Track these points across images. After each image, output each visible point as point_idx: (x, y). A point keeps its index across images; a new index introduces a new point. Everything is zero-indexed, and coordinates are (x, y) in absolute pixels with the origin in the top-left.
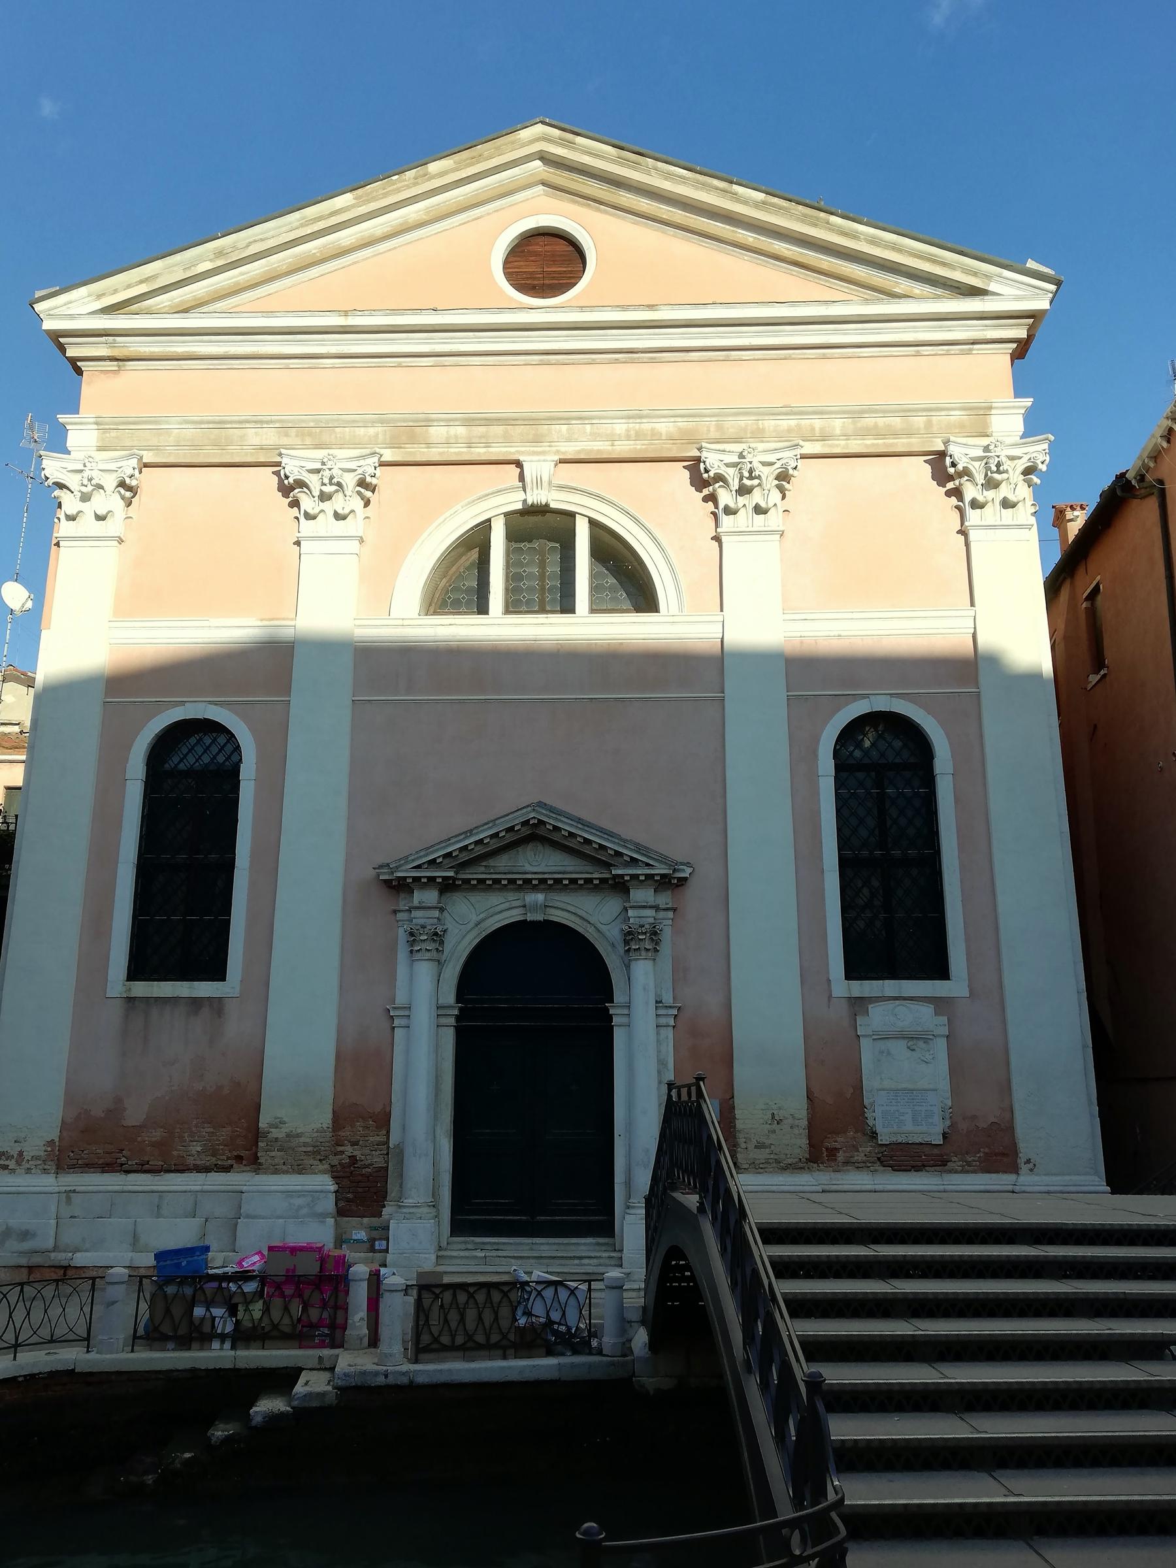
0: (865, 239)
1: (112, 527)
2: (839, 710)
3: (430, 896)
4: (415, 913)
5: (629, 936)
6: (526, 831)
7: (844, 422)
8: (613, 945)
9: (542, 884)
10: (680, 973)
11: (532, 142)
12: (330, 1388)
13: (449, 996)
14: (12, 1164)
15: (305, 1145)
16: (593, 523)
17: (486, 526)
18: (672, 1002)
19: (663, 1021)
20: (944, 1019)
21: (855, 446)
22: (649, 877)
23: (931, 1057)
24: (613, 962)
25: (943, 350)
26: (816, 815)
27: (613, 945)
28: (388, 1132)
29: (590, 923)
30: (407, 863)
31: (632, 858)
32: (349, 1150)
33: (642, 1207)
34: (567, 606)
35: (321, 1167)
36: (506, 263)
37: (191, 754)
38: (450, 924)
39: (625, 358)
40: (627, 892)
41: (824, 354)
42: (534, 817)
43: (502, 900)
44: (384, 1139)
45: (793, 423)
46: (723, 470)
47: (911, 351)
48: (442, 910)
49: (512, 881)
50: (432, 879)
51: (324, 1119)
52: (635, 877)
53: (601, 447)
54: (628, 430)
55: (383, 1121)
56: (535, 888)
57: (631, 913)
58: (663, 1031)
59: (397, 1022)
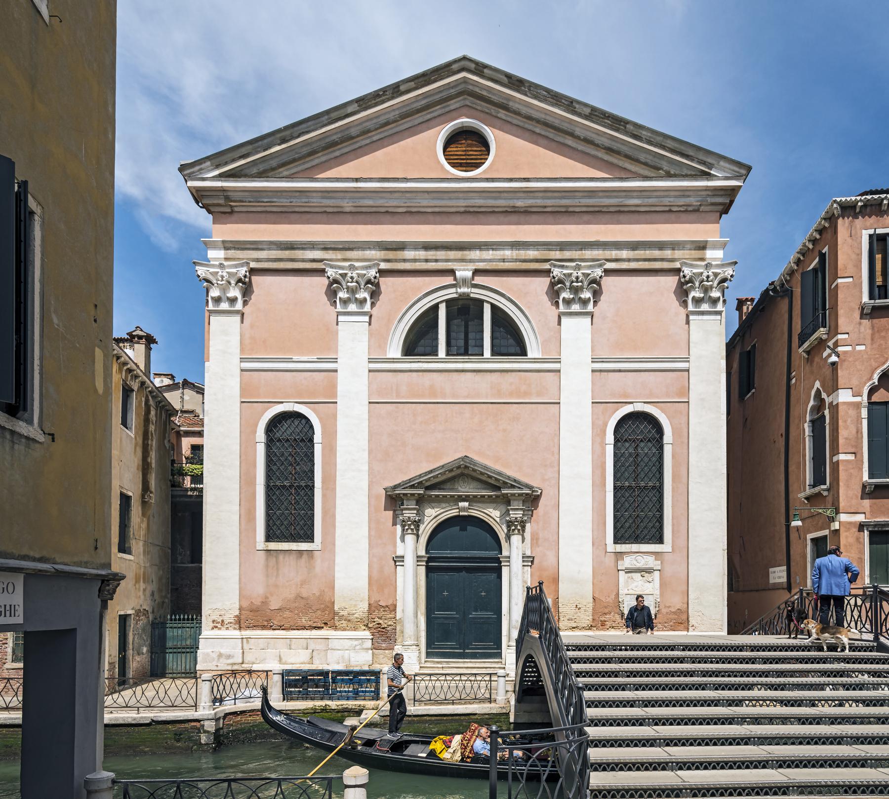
6: (459, 471)
14: (219, 625)
17: (435, 308)
26: (604, 464)
50: (413, 495)
51: (365, 606)
52: (513, 495)
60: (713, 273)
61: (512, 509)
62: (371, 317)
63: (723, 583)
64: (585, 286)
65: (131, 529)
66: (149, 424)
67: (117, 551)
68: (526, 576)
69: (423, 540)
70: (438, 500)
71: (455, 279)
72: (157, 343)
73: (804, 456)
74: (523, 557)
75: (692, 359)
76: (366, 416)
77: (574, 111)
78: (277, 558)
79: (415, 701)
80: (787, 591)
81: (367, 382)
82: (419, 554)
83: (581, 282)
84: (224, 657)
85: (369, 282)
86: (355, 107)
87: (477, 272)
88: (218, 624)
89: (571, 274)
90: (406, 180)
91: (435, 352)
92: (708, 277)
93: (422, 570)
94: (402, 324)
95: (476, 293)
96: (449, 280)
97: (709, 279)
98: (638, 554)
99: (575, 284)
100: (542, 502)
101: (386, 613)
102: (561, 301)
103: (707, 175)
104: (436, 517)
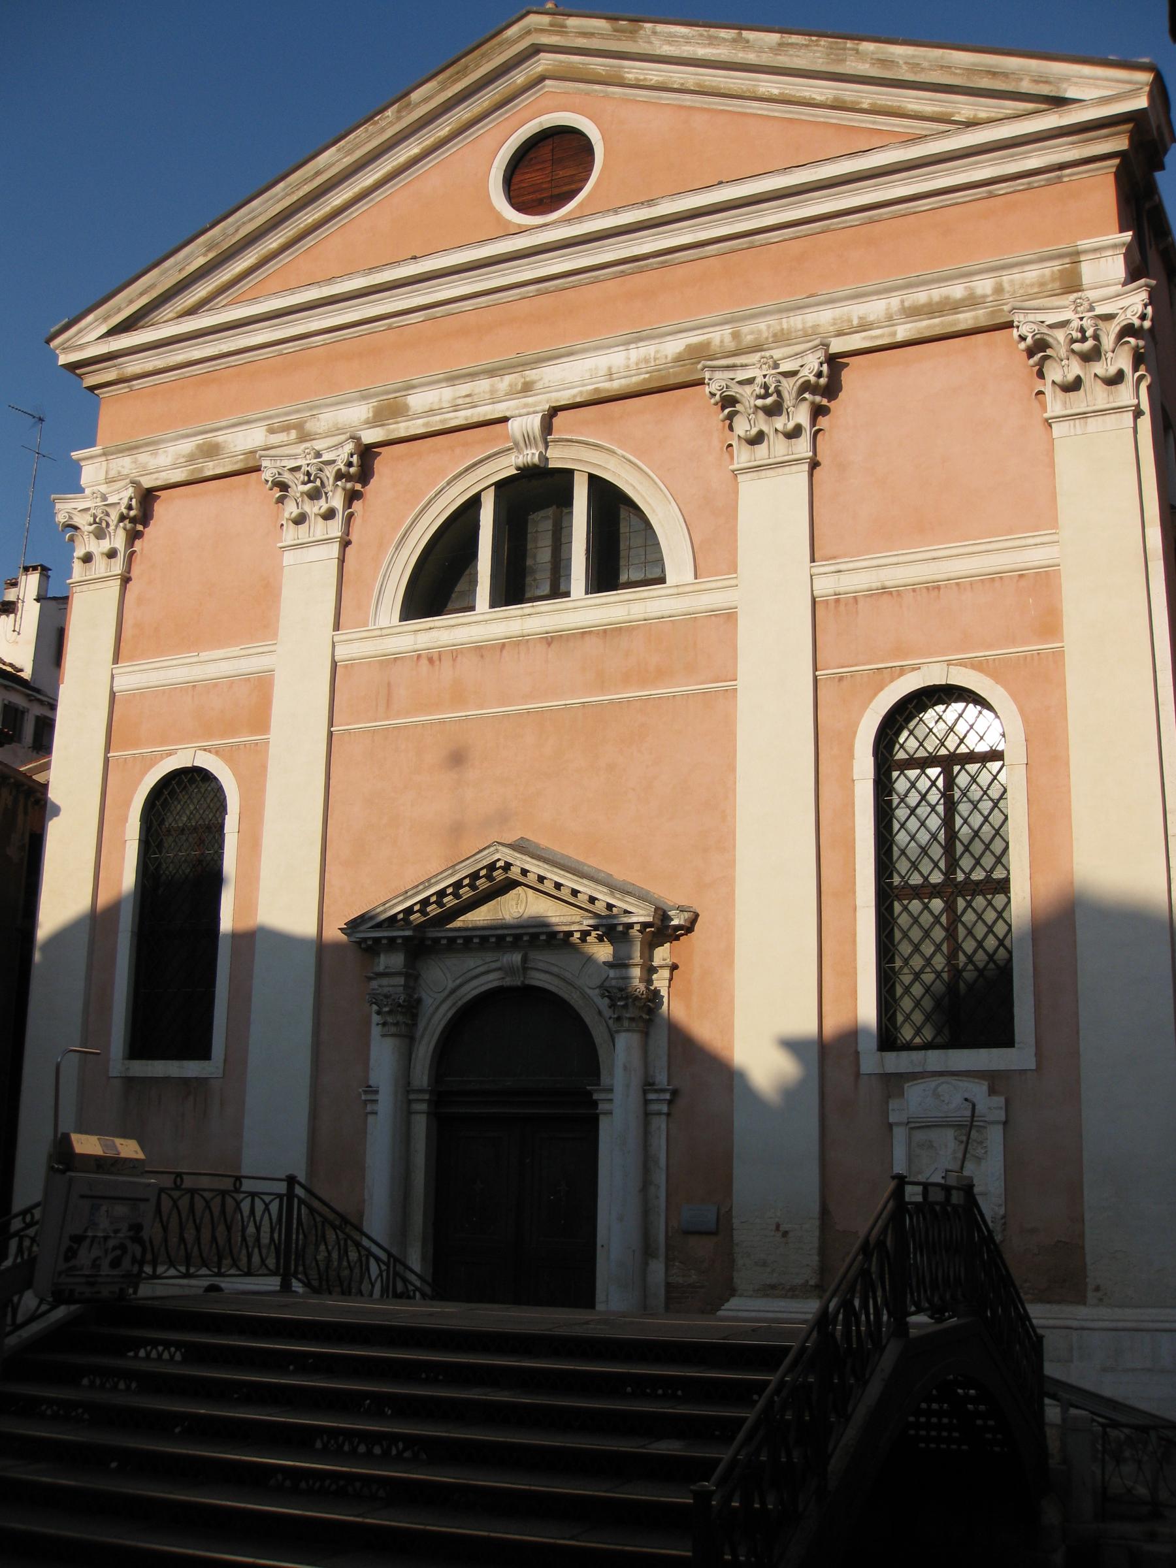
2: (882, 689)
7: (889, 303)
11: (521, 37)
16: (593, 479)
17: (474, 503)
18: (666, 1084)
20: (999, 1100)
23: (983, 1152)
24: (599, 1034)
25: (1023, 184)
29: (575, 988)
33: (423, 1100)
34: (558, 590)
37: (907, 1012)
39: (630, 269)
41: (870, 217)
43: (480, 962)
47: (983, 192)
50: (392, 940)
69: (424, 1051)
94: (405, 552)
98: (942, 1079)
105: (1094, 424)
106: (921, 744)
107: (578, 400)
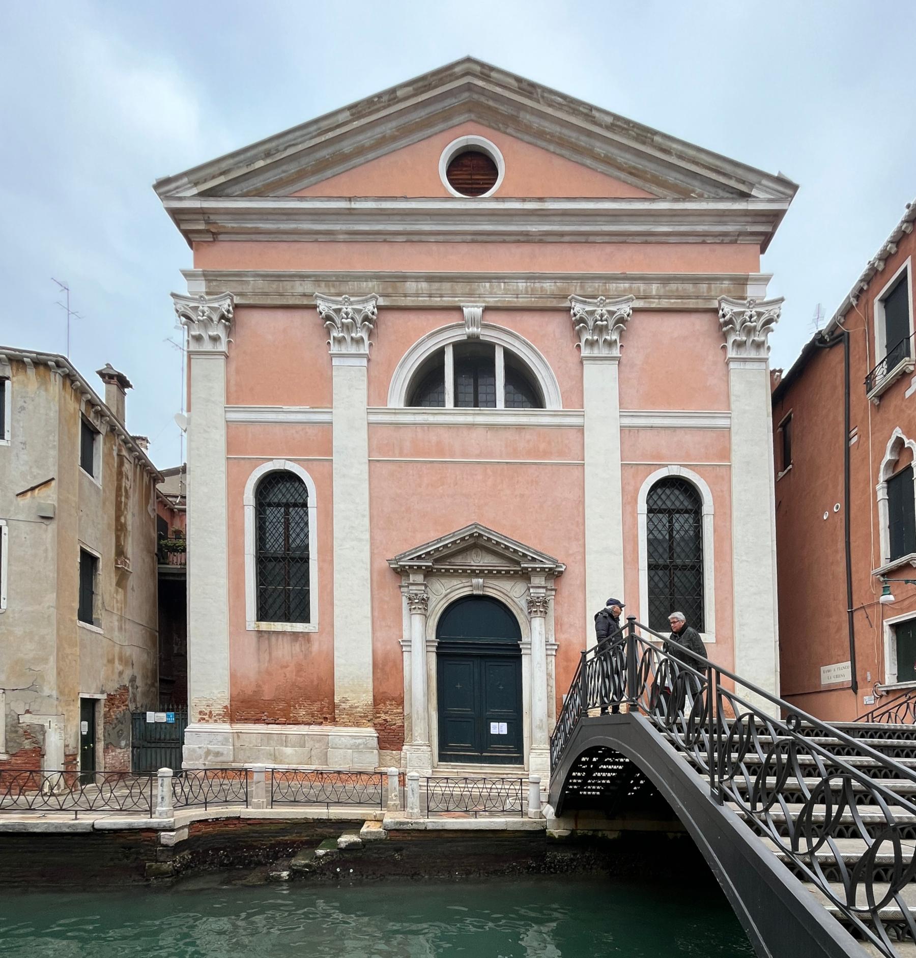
0: (676, 154)
1: (222, 347)
3: (419, 578)
4: (411, 587)
5: (531, 603)
6: (472, 541)
8: (521, 610)
9: (480, 573)
10: (559, 624)
12: (381, 830)
13: (433, 637)
14: (206, 717)
15: (360, 712)
17: (440, 353)
19: (549, 652)
21: (665, 303)
22: (543, 569)
24: (521, 619)
26: (636, 537)
27: (521, 610)
28: (403, 707)
30: (405, 557)
31: (532, 557)
32: (383, 716)
33: (433, 646)
35: (369, 724)
36: (449, 173)
38: (430, 596)
40: (529, 579)
42: (476, 532)
44: (401, 711)
45: (627, 285)
46: (585, 316)
48: (426, 586)
49: (464, 571)
50: (419, 567)
51: (368, 698)
52: (534, 569)
53: (510, 300)
54: (527, 287)
55: (400, 702)
56: (477, 576)
57: (532, 590)
58: (550, 658)
59: (404, 650)
60: (756, 312)
61: (532, 587)
62: (369, 360)
63: (776, 680)
64: (610, 327)
65: (100, 598)
66: (122, 478)
67: (77, 618)
68: (550, 668)
70: (447, 574)
71: (463, 319)
72: (131, 386)
73: (877, 524)
74: (546, 645)
75: (734, 415)
76: (366, 476)
77: (594, 121)
78: (269, 639)
79: (428, 811)
80: (851, 691)
81: (366, 437)
82: (428, 638)
83: (606, 320)
84: (212, 754)
85: (366, 318)
86: (346, 116)
87: (487, 309)
88: (205, 716)
89: (595, 311)
90: (405, 198)
91: (442, 403)
92: (751, 317)
93: (433, 658)
94: (405, 371)
95: (487, 335)
96: (453, 319)
97: (752, 319)
99: (599, 323)
100: (566, 580)
101: (392, 707)
102: (582, 344)
103: (745, 196)
104: (446, 596)
105: (749, 366)
106: (655, 502)
107: (499, 305)
